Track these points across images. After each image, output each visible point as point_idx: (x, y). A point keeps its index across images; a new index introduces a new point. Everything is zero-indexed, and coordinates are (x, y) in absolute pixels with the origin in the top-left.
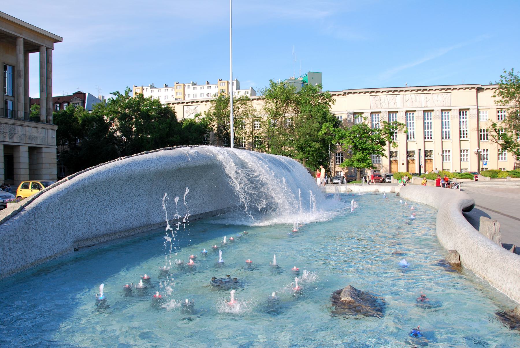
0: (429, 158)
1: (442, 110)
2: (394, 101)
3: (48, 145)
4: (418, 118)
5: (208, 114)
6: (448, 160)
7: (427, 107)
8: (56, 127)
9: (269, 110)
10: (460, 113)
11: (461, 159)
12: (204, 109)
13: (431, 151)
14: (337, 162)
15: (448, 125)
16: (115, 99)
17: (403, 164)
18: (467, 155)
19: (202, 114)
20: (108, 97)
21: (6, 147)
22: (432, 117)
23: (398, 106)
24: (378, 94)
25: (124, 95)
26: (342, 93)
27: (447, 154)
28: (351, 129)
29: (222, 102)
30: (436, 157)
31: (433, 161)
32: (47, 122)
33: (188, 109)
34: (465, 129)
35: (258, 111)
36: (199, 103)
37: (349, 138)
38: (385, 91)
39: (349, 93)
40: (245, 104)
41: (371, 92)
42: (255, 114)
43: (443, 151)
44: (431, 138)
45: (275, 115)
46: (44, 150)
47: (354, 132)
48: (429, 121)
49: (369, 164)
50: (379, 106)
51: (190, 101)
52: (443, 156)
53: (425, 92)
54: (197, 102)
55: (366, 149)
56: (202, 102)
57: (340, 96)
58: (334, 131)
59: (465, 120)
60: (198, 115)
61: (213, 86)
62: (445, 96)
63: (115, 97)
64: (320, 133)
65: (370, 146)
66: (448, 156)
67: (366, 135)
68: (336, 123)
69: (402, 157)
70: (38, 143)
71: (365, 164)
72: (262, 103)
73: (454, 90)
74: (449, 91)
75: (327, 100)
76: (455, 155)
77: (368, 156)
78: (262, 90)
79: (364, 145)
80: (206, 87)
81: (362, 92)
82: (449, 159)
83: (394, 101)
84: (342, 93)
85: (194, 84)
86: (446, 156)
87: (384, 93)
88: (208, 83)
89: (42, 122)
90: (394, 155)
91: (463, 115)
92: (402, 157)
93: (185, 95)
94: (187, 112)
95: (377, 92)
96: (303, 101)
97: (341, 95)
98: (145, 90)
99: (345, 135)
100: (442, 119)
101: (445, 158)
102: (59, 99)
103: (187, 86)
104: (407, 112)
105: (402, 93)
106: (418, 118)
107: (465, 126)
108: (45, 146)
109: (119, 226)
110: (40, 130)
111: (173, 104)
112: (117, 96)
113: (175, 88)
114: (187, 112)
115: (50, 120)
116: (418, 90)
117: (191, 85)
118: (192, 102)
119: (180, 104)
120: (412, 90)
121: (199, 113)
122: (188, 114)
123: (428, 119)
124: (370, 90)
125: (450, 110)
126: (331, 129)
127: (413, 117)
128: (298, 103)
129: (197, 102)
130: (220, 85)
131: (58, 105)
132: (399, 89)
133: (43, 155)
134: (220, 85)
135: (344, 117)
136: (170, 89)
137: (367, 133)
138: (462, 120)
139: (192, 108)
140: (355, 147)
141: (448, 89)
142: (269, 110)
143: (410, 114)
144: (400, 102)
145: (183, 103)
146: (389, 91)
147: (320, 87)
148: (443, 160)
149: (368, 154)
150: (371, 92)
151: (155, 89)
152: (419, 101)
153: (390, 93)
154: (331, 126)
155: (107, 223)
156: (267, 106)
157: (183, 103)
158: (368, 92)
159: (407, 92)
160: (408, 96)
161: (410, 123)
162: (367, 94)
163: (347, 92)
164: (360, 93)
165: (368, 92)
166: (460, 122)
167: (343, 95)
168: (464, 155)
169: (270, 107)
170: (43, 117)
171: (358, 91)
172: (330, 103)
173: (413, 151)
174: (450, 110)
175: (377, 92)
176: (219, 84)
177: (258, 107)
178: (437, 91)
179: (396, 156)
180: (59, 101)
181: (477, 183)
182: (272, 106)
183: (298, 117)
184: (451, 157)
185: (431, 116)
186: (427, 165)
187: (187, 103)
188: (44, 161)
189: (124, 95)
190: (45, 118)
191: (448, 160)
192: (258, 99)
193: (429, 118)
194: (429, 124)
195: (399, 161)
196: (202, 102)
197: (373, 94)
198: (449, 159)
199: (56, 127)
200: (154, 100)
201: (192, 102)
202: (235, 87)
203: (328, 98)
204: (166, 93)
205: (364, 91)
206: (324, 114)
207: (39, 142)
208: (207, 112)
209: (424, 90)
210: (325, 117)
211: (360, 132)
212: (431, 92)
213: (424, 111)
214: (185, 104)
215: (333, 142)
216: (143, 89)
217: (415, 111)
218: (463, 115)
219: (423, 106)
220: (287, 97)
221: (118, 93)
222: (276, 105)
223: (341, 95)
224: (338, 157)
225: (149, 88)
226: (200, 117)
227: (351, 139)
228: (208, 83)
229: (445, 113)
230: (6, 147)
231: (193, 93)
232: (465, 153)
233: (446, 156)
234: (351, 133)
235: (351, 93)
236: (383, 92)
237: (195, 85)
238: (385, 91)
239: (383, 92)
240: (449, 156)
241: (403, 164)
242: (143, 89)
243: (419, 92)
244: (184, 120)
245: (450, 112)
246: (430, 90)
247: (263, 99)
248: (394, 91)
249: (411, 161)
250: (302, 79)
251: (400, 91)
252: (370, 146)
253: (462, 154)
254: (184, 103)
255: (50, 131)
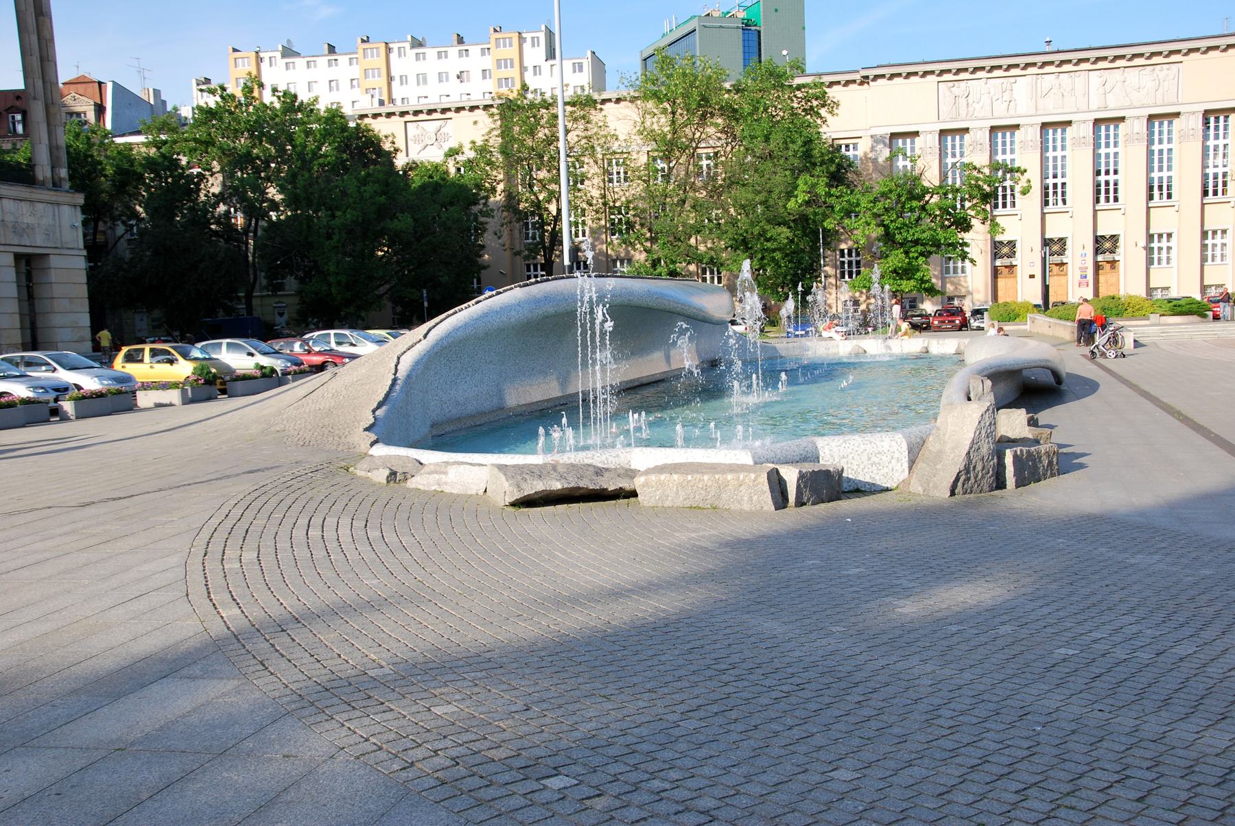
0: (1108, 256)
1: (1151, 118)
2: (1007, 96)
3: (62, 249)
4: (1078, 142)
5: (483, 150)
6: (1164, 261)
7: (1106, 109)
8: (80, 199)
9: (651, 136)
10: (1206, 123)
11: (1204, 259)
12: (472, 132)
13: (1114, 238)
14: (843, 276)
15: (1169, 160)
16: (213, 106)
17: (1032, 276)
18: (1224, 245)
19: (466, 149)
20: (187, 102)
21: (18, 257)
22: (1121, 139)
23: (1020, 111)
24: (963, 76)
25: (239, 94)
26: (857, 77)
27: (1164, 244)
28: (878, 189)
29: (516, 112)
30: (1130, 255)
31: (1121, 265)
32: (54, 185)
33: (419, 132)
34: (1220, 171)
35: (622, 137)
36: (448, 115)
37: (869, 214)
38: (983, 68)
39: (876, 77)
40: (583, 117)
41: (942, 72)
42: (615, 147)
43: (1150, 238)
44: (1116, 199)
45: (669, 147)
46: (54, 261)
47: (884, 195)
48: (1112, 150)
49: (922, 281)
50: (963, 112)
51: (425, 108)
52: (1150, 250)
53: (1101, 65)
54: (444, 111)
55: (916, 242)
56: (458, 110)
57: (852, 86)
58: (829, 195)
59: (1221, 142)
60: (452, 153)
61: (475, 50)
62: (1162, 75)
63: (212, 101)
64: (791, 204)
65: (925, 235)
66: (1165, 250)
67: (915, 203)
68: (839, 170)
69: (1028, 258)
70: (37, 242)
71: (912, 283)
72: (626, 109)
73: (1192, 55)
74: (1174, 58)
75: (815, 103)
76: (1186, 246)
77: (921, 260)
78: (633, 79)
79: (911, 232)
80: (454, 51)
81: (916, 74)
82: (1168, 259)
83: (1007, 96)
84: (857, 77)
85: (417, 44)
86: (1160, 249)
87: (979, 74)
88: (460, 41)
89: (42, 185)
90: (1005, 250)
91: (1217, 128)
92: (1028, 258)
93: (390, 79)
94: (417, 140)
95: (959, 71)
96: (747, 109)
97: (854, 81)
98: (266, 61)
99: (858, 205)
100: (1150, 142)
101: (1156, 256)
102: (18, 98)
103: (396, 51)
104: (1045, 126)
105: (1031, 70)
106: (1078, 142)
107: (1220, 161)
108: (57, 251)
109: (471, 408)
110: (40, 206)
111: (375, 116)
112: (218, 99)
113: (360, 55)
114: (417, 140)
115: (60, 179)
116: (1080, 61)
117: (408, 45)
118: (430, 112)
119: (393, 118)
120: (1062, 62)
121: (455, 145)
122: (419, 147)
123: (1107, 145)
124: (937, 67)
125: (1177, 115)
126: (821, 190)
127: (1063, 139)
128: (732, 113)
129: (444, 111)
130: (498, 46)
131: (19, 117)
132: (1022, 61)
133: (53, 276)
134: (498, 46)
135: (863, 147)
136: (343, 60)
137: (920, 198)
138: (1211, 143)
139: (431, 127)
140: (888, 237)
141: (1171, 53)
142: (651, 136)
143: (1055, 132)
144: (1025, 98)
145: (403, 114)
146: (993, 68)
147: (799, 68)
148: (1150, 262)
149: (922, 254)
150: (942, 72)
151: (297, 60)
152: (1081, 94)
153: (996, 73)
154: (824, 180)
155: (458, 403)
156: (648, 124)
157: (403, 114)
158: (932, 72)
159: (1048, 69)
160: (1050, 80)
161: (1055, 159)
162: (929, 78)
163: (871, 73)
164: (909, 75)
165: (932, 72)
166: (1205, 149)
167: (862, 83)
168: (1214, 245)
169: (655, 127)
170: (43, 171)
171: (905, 70)
172: (823, 112)
173: (1061, 240)
174: (1177, 115)
175: (959, 71)
176: (493, 41)
177: (623, 123)
178: (1138, 61)
179: (1012, 254)
180: (18, 103)
181: (1218, 325)
182: (661, 124)
183: (732, 153)
184: (1173, 254)
185: (1116, 136)
186: (1102, 278)
187: (416, 113)
188: (57, 291)
189: (239, 94)
190: (49, 174)
191: (1164, 261)
192: (618, 101)
193: (1112, 140)
194: (1059, 190)
195: (1019, 269)
196: (458, 110)
197: (946, 77)
198: (1168, 259)
199: (80, 199)
200: (328, 110)
201: (430, 112)
202: (541, 50)
203: (818, 100)
204: (333, 73)
205: (921, 69)
206: (805, 143)
207: (39, 241)
208: (479, 143)
209: (1098, 59)
210: (807, 155)
211: (899, 196)
212: (1119, 63)
213: (1097, 122)
214: (408, 118)
215: (829, 224)
216: (259, 60)
217: (1069, 123)
218: (1217, 128)
219: (1093, 106)
220: (704, 98)
221: (223, 89)
222: (673, 122)
223: (854, 81)
224: (846, 259)
225: (278, 55)
226: (460, 158)
227: (876, 216)
228: (460, 41)
229: (1161, 124)
230: (18, 257)
231: (426, 76)
232: (1218, 240)
233: (1160, 249)
234: (875, 201)
235: (883, 76)
236: (976, 69)
237: (420, 45)
238: (983, 68)
239: (976, 69)
240: (1169, 248)
241: (1032, 276)
242: (259, 60)
243: (1084, 66)
244: (412, 166)
245: (1176, 121)
246: (1116, 58)
247: (633, 100)
248: (1010, 67)
249: (1055, 269)
250: (741, 15)
251: (1027, 65)
252: (925, 235)
253: (1209, 242)
254: (407, 113)
255: (66, 210)
